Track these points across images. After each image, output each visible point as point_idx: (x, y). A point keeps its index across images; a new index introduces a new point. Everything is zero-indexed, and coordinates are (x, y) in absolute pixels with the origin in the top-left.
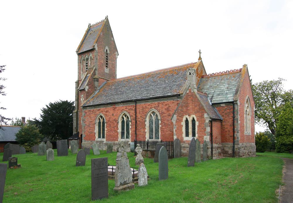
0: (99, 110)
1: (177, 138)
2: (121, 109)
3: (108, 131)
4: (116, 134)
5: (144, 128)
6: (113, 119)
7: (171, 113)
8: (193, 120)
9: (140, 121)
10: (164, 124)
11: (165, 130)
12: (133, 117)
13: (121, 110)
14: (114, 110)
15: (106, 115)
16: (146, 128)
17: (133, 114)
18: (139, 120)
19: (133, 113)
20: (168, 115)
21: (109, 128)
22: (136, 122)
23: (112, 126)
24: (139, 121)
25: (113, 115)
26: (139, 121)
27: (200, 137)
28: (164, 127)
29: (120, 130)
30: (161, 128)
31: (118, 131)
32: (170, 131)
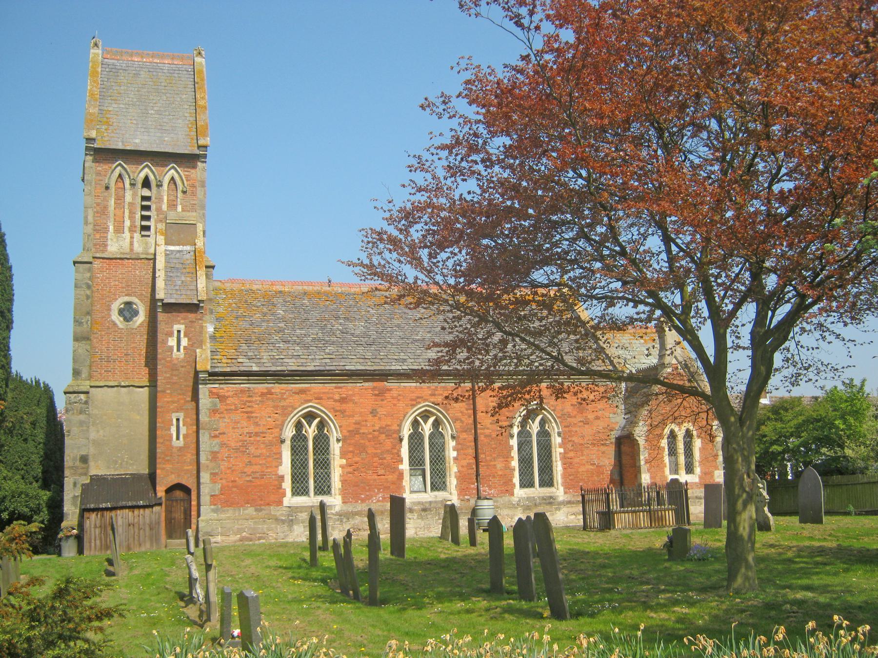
0: (302, 392)
1: (651, 478)
2: (414, 396)
3: (350, 469)
4: (391, 477)
5: (508, 458)
6: (377, 428)
7: (589, 417)
8: (688, 434)
9: (490, 436)
10: (572, 446)
11: (577, 460)
12: (462, 422)
13: (412, 400)
14: (376, 395)
15: (343, 412)
16: (513, 457)
17: (461, 412)
18: (487, 432)
19: (463, 410)
20: (583, 421)
21: (356, 459)
22: (476, 440)
23: (371, 450)
24: (486, 436)
25: (374, 412)
26: (486, 436)
27: (706, 474)
28: (571, 454)
29: (286, 468)
30: (564, 457)
31: (401, 467)
32: (591, 464)
